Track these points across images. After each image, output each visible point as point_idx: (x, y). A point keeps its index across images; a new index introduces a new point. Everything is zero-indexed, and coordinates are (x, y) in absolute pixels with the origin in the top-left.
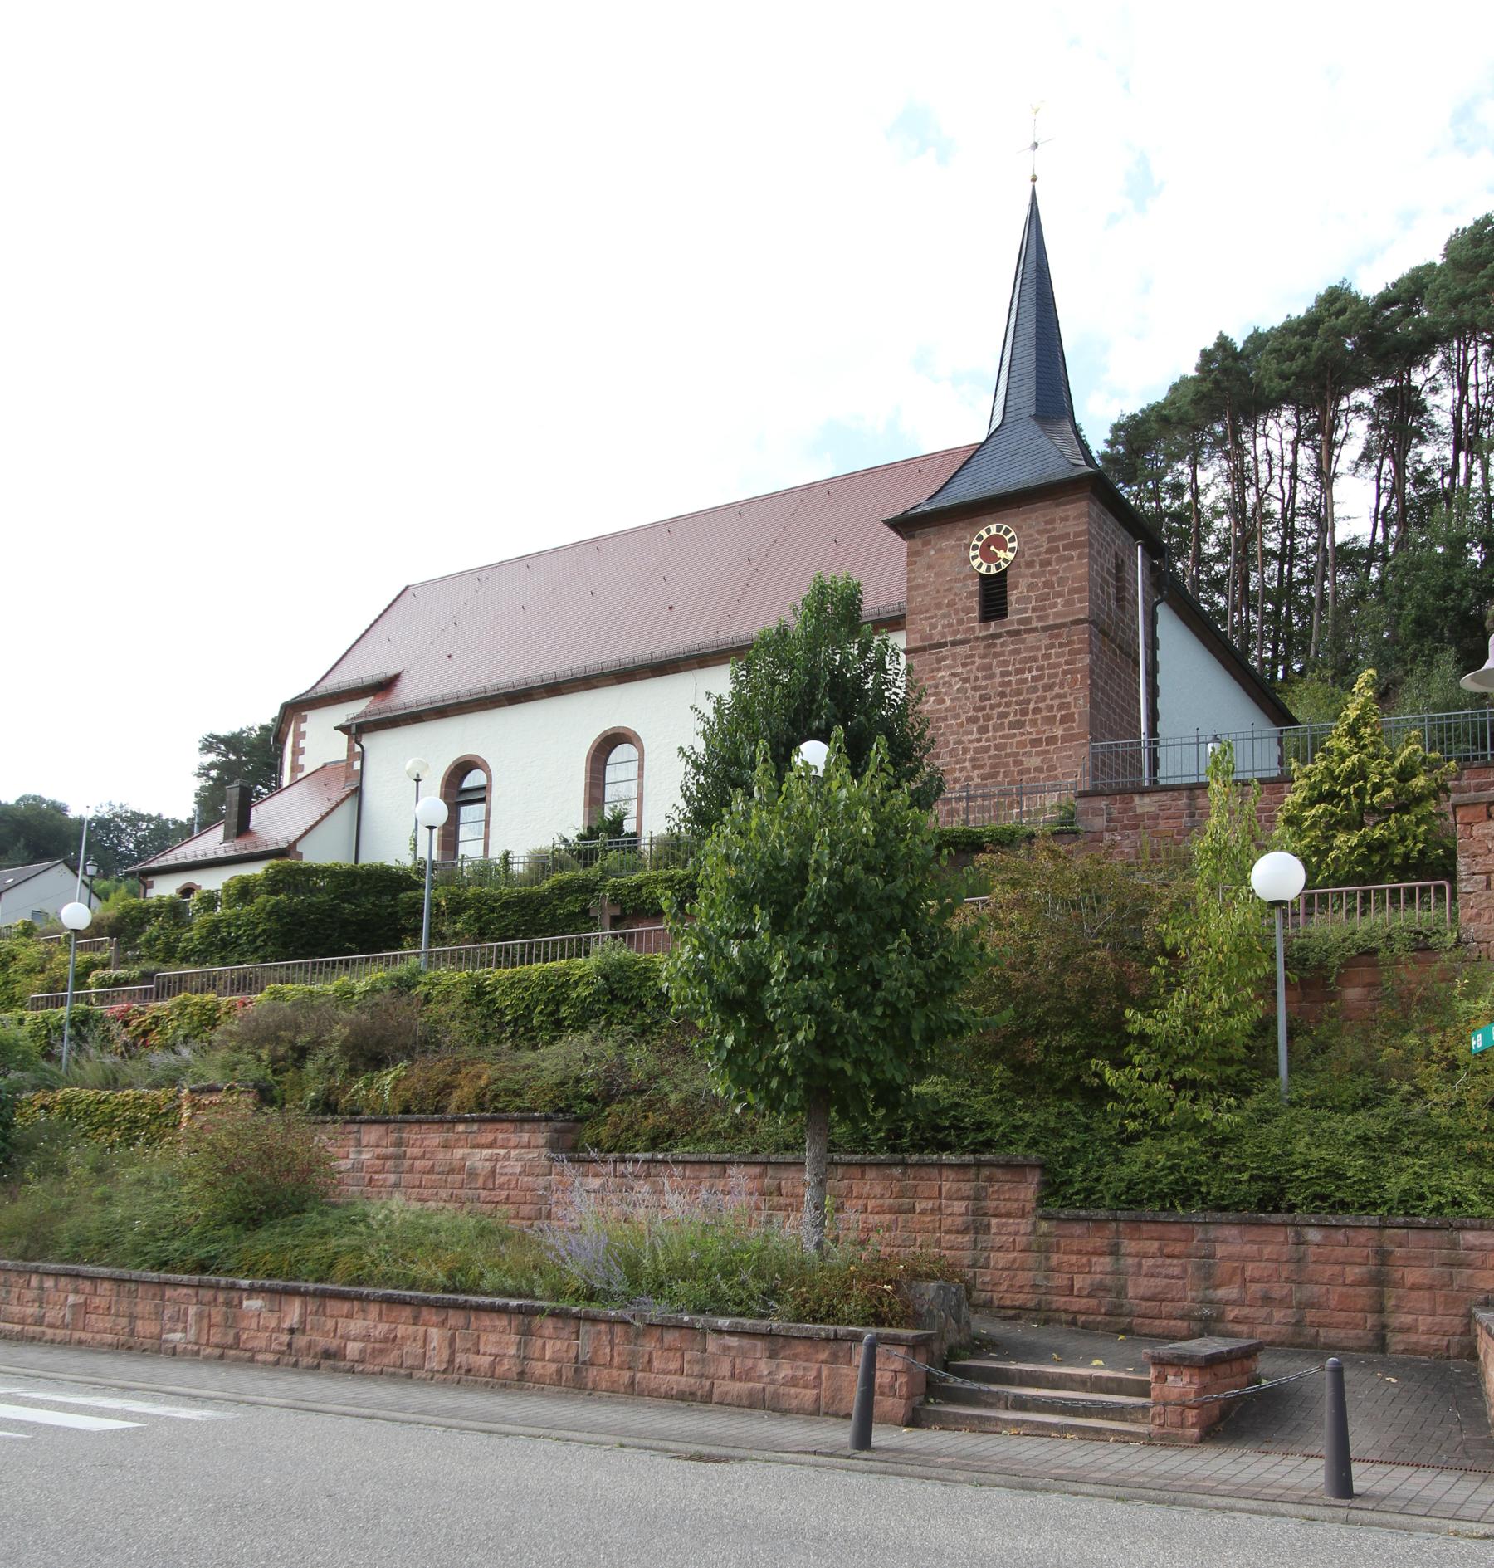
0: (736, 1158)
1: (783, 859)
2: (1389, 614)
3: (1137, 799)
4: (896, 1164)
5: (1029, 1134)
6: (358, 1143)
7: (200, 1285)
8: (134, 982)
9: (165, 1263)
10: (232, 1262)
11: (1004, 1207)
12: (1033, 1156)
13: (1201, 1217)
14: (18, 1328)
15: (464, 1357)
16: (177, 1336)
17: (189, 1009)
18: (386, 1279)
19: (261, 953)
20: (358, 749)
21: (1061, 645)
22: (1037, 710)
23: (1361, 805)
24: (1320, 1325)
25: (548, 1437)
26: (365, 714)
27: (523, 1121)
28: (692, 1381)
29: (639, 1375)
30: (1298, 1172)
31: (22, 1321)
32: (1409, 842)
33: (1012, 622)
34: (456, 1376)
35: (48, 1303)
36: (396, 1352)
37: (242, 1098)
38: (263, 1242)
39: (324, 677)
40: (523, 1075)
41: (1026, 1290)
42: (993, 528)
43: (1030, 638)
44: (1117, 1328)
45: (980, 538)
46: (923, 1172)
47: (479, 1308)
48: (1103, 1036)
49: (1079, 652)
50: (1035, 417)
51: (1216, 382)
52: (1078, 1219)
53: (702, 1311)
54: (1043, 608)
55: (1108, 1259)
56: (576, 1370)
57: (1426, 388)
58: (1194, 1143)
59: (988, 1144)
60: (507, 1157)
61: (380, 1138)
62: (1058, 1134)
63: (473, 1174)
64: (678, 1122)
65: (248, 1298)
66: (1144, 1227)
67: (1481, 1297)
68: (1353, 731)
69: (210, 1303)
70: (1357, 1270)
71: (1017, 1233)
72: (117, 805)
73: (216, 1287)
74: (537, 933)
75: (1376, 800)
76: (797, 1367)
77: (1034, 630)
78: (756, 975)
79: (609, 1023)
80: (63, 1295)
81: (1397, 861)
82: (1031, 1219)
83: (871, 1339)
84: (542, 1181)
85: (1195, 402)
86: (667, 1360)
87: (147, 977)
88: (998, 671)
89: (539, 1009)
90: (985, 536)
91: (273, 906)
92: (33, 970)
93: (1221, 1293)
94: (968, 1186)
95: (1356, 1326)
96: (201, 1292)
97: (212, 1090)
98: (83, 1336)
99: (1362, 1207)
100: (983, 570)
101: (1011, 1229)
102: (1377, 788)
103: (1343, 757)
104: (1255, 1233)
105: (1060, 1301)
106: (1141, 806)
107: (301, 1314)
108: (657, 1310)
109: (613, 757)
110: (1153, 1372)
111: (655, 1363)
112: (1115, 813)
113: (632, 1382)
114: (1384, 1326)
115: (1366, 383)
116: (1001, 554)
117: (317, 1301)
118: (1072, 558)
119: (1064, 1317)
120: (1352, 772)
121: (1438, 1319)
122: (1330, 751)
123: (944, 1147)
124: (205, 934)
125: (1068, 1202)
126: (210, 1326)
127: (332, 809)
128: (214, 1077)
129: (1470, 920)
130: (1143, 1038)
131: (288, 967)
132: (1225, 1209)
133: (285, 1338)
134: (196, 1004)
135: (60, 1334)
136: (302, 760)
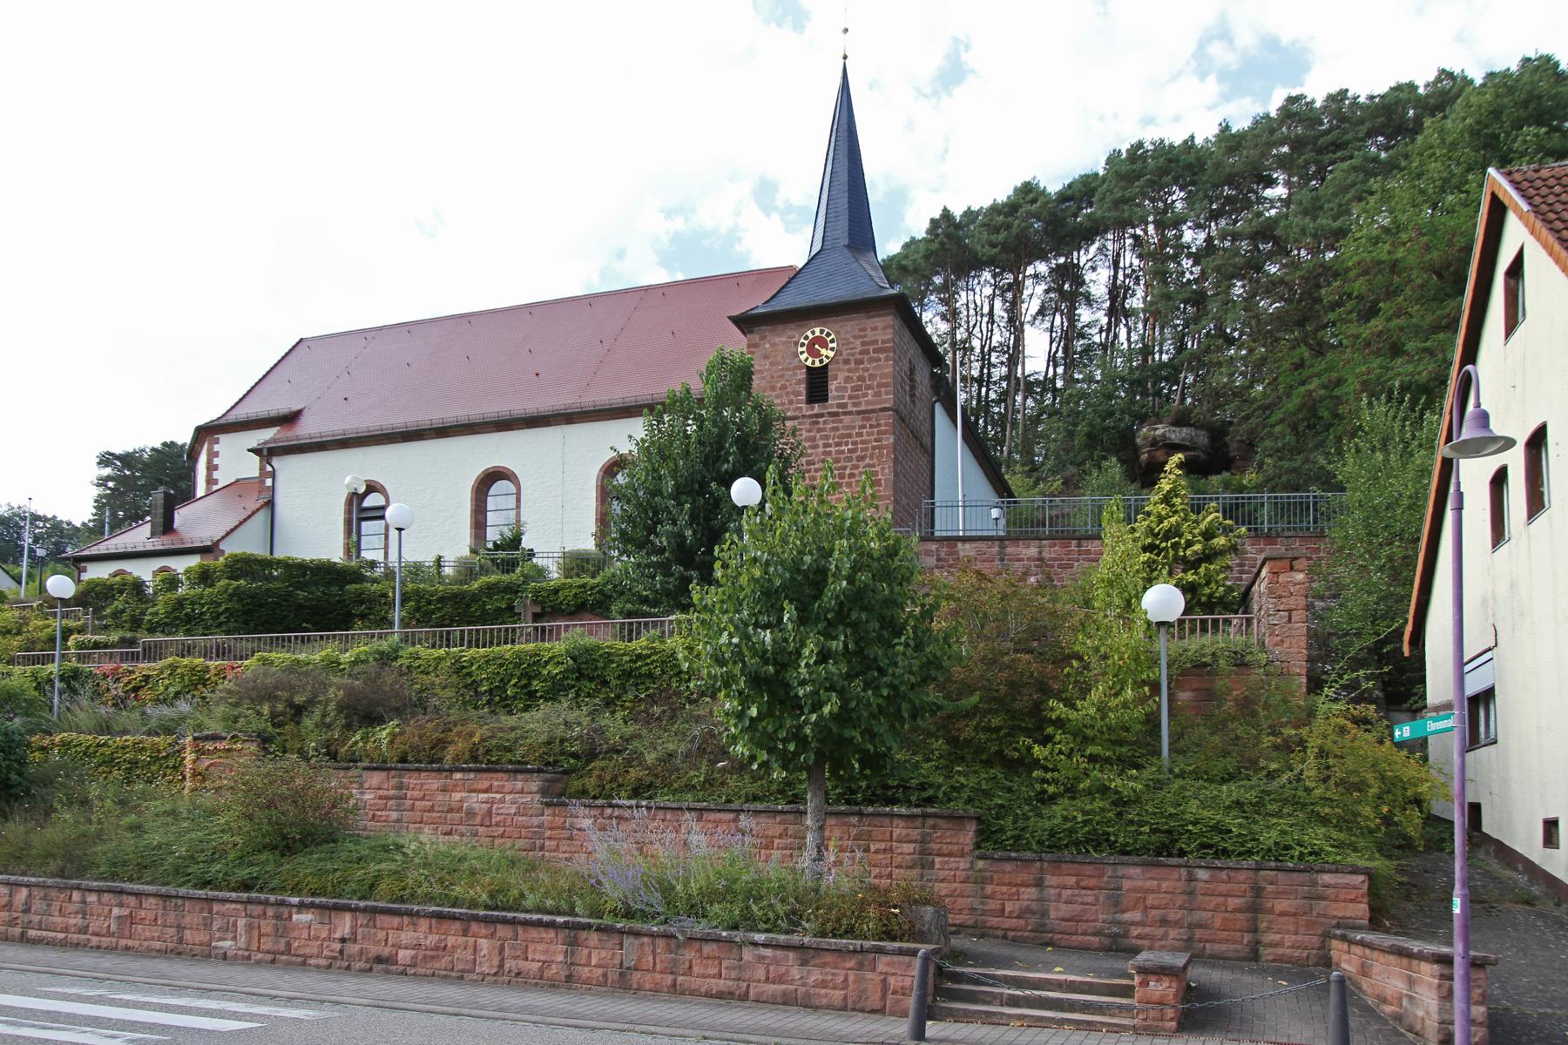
0: (713, 807)
1: (804, 564)
2: (1066, 430)
3: (960, 545)
4: (853, 814)
5: (965, 794)
6: (361, 786)
7: (249, 901)
8: (113, 646)
9: (209, 883)
10: (275, 883)
11: (946, 849)
12: (972, 811)
13: (1112, 859)
14: (61, 936)
15: (514, 963)
16: (228, 943)
17: (179, 671)
18: (429, 898)
19: (224, 628)
20: (269, 469)
21: (871, 426)
22: (852, 475)
23: (1176, 555)
24: (1206, 941)
25: (633, 1031)
26: (273, 440)
27: (516, 771)
28: (730, 983)
29: (680, 979)
30: (1190, 827)
31: (66, 930)
32: (1213, 585)
33: (832, 406)
34: (506, 978)
35: (91, 915)
36: (447, 959)
37: (247, 745)
38: (305, 865)
39: (233, 408)
40: (513, 735)
41: (966, 912)
42: (817, 331)
43: (846, 419)
44: (1041, 941)
45: (807, 337)
46: (877, 821)
47: (527, 924)
48: (1024, 720)
49: (885, 432)
50: (848, 247)
51: (942, 244)
52: (1009, 859)
53: (735, 927)
54: (857, 397)
55: (1034, 890)
56: (621, 974)
57: (1087, 267)
58: (1098, 804)
59: (930, 801)
60: (502, 801)
61: (382, 782)
62: (988, 794)
63: (471, 814)
64: (657, 776)
65: (298, 913)
66: (1064, 866)
67: (1335, 922)
68: (1166, 500)
69: (259, 917)
70: (1237, 901)
71: (957, 869)
72: (16, 506)
73: (266, 903)
74: (469, 624)
75: (1188, 552)
76: (826, 974)
77: (850, 413)
78: (784, 659)
79: (578, 695)
80: (107, 908)
81: (1204, 599)
82: (969, 859)
83: (925, 953)
84: (535, 821)
85: (927, 257)
86: (706, 967)
87: (124, 642)
88: (821, 443)
89: (513, 682)
90: (811, 336)
91: (235, 589)
92: (9, 632)
93: (1127, 916)
94: (916, 832)
95: (1235, 942)
96: (250, 907)
97: (215, 738)
98: (130, 943)
99: (1240, 854)
100: (809, 363)
101: (953, 865)
102: (1189, 544)
103: (1161, 520)
104: (1155, 872)
105: (994, 921)
106: (964, 550)
107: (352, 927)
108: (701, 928)
109: (493, 491)
110: (1137, 979)
111: (696, 969)
112: (943, 555)
113: (674, 985)
114: (1258, 942)
115: (1044, 258)
116: (823, 351)
117: (368, 916)
118: (879, 360)
119: (1000, 933)
120: (1169, 531)
121: (1300, 938)
122: (1149, 514)
123: (893, 801)
124: (170, 609)
125: (999, 844)
126: (260, 936)
127: (249, 517)
128: (214, 727)
129: (1276, 645)
130: (1060, 723)
131: (247, 639)
132: (1127, 853)
133: (337, 946)
134: (186, 666)
135: (106, 941)
136: (216, 475)
